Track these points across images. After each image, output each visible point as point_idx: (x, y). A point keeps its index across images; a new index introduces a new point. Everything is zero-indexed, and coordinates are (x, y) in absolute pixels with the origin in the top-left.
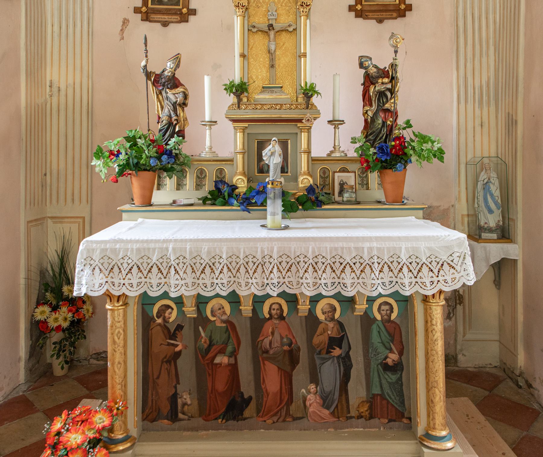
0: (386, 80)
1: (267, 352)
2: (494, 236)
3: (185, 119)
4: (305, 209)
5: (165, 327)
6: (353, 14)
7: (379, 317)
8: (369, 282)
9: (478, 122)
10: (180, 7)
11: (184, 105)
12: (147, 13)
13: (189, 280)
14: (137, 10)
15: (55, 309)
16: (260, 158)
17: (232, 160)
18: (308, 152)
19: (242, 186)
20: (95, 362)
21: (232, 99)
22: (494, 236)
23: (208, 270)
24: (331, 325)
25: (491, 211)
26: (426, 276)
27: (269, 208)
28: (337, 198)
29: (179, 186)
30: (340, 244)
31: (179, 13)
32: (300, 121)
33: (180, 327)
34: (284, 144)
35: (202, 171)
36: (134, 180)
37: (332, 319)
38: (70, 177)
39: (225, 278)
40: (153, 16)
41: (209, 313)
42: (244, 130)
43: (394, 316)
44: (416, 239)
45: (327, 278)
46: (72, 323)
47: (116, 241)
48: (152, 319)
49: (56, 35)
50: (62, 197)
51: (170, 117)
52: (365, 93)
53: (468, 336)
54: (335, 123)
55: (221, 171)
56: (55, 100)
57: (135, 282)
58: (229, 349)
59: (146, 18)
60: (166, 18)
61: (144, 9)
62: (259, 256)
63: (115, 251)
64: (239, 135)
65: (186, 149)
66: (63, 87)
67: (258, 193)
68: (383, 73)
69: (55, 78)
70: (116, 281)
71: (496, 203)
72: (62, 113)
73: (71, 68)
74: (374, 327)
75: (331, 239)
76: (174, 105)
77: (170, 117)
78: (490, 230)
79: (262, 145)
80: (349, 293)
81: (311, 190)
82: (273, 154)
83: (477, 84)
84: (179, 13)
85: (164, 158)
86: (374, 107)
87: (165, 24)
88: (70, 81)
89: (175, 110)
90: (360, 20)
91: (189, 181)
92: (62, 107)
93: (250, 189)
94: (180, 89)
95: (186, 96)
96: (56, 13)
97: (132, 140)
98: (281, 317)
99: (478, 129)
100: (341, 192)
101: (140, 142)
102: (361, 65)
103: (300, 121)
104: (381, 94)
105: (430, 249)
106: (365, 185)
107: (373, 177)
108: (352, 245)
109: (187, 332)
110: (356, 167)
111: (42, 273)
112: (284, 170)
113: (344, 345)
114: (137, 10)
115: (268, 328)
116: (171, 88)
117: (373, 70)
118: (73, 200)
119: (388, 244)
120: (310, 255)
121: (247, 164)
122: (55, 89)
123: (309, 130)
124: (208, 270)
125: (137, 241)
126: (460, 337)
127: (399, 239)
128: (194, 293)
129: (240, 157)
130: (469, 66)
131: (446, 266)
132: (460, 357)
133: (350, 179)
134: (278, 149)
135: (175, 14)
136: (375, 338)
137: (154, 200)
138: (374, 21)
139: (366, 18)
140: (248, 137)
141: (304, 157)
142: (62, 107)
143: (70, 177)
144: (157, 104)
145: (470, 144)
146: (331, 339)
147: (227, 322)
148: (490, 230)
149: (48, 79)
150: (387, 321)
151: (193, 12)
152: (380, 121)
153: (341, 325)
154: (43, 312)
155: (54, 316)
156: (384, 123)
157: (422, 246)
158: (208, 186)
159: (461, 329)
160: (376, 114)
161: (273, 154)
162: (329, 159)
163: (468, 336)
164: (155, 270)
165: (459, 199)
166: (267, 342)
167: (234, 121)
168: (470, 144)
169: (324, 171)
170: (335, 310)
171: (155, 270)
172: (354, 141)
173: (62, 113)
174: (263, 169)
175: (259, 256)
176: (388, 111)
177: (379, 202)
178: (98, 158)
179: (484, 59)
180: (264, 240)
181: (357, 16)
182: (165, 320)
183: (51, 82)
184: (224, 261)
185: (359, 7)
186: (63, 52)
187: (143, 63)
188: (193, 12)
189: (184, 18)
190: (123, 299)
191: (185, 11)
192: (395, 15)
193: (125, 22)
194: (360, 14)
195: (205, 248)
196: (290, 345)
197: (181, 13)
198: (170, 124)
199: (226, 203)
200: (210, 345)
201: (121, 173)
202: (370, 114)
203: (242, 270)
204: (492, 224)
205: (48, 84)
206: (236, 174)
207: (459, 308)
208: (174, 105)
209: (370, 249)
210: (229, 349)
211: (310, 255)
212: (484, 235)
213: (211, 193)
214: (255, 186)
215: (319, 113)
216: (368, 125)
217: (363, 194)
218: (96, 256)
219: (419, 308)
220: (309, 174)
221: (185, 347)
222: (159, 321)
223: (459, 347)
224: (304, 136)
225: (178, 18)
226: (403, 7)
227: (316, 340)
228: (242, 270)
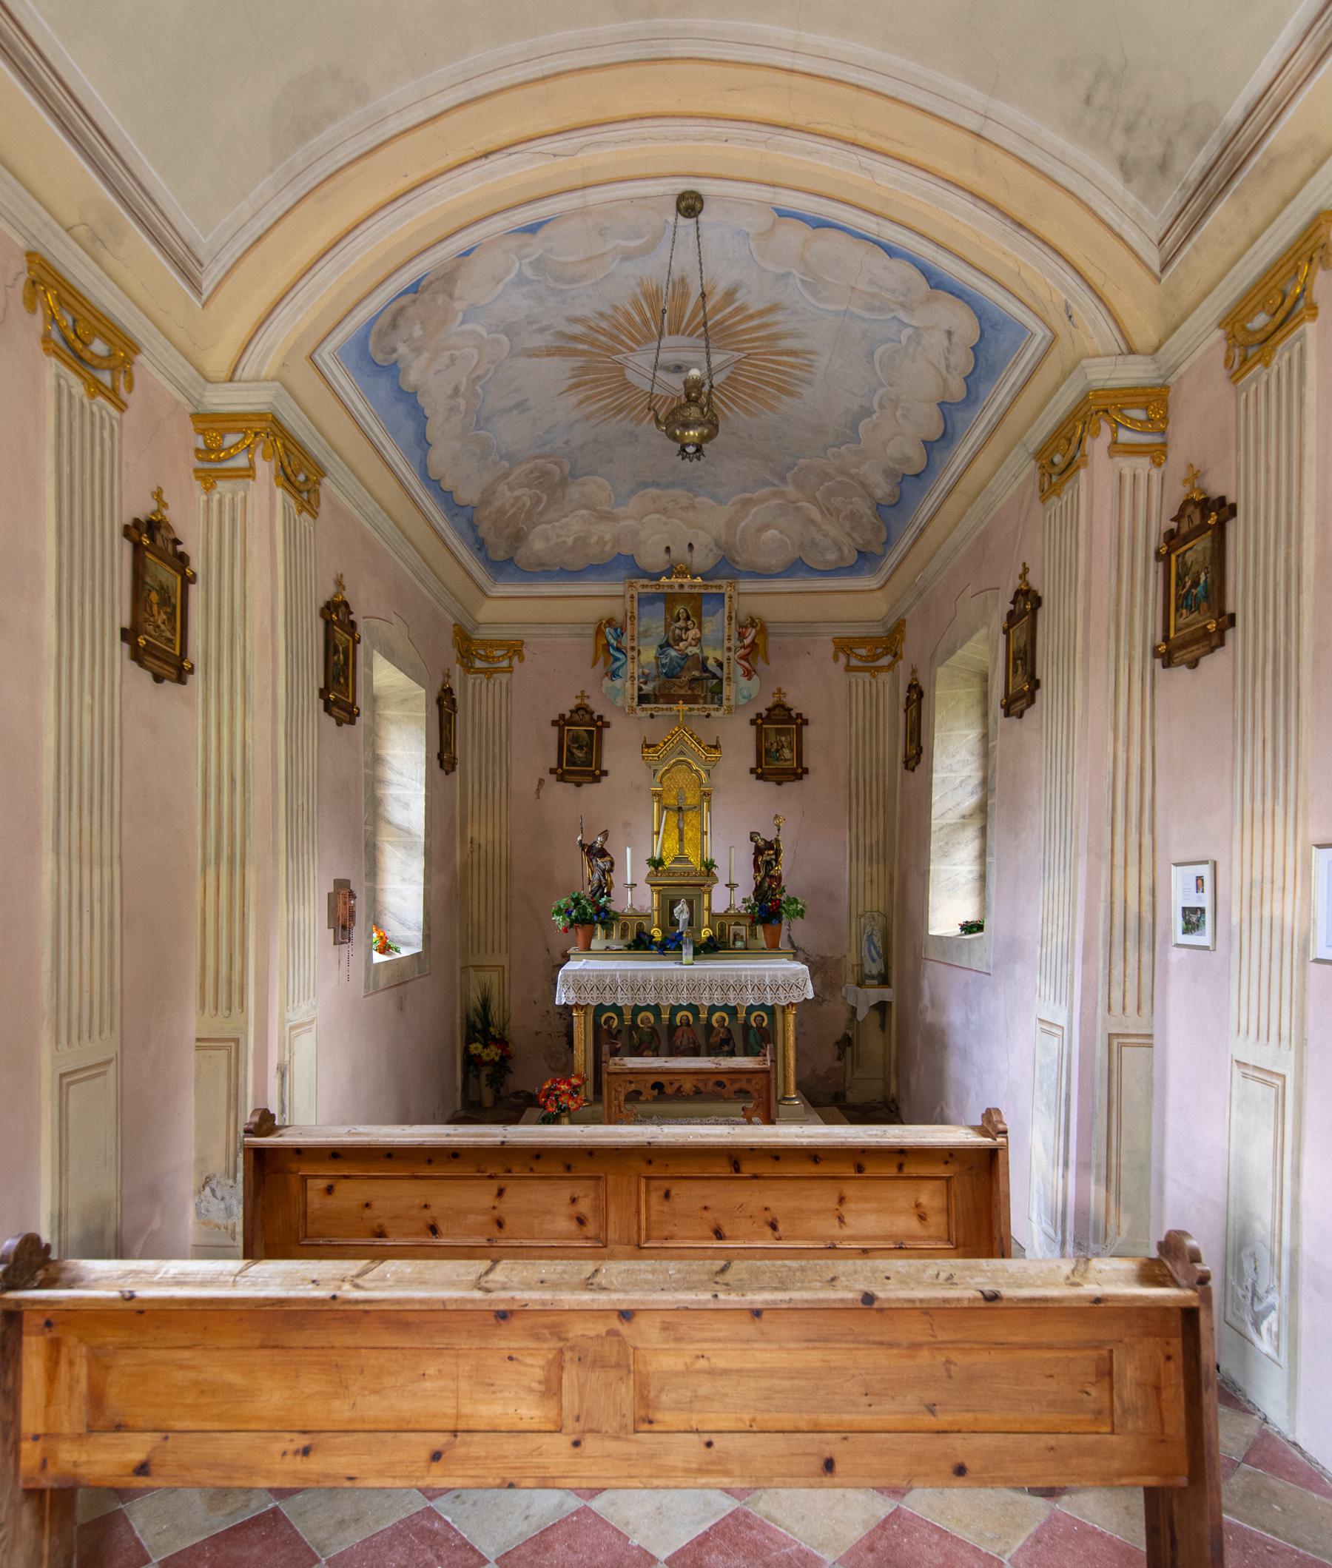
0: (771, 852)
1: (678, 1048)
2: (876, 982)
3: (612, 882)
4: (706, 953)
5: (609, 1031)
6: (754, 776)
7: (754, 1025)
8: (745, 997)
9: (868, 878)
10: (593, 768)
11: (611, 870)
12: (562, 774)
13: (630, 996)
14: (552, 771)
15: (485, 1046)
16: (672, 913)
17: (649, 916)
18: (709, 909)
19: (657, 934)
20: (515, 1100)
21: (650, 869)
22: (876, 982)
23: (642, 989)
24: (722, 1030)
25: (873, 960)
26: (781, 993)
27: (684, 951)
28: (732, 946)
29: (608, 936)
30: (727, 973)
31: (592, 774)
32: (703, 885)
33: (619, 1031)
34: (690, 903)
35: (625, 925)
36: (579, 931)
37: (723, 1026)
38: (490, 928)
39: (653, 994)
40: (568, 777)
41: (639, 1022)
42: (659, 892)
43: (764, 1024)
44: (776, 969)
45: (717, 995)
46: (502, 1057)
47: (583, 970)
48: (601, 1026)
49: (476, 795)
50: (489, 948)
51: (600, 880)
52: (755, 861)
53: (856, 1075)
54: (731, 886)
55: (640, 924)
56: (476, 855)
57: (595, 996)
58: (653, 1046)
59: (561, 778)
60: (580, 779)
61: (560, 771)
62: (675, 980)
63: (581, 976)
64: (655, 896)
65: (615, 907)
66: (483, 843)
67: (672, 941)
68: (769, 845)
69: (476, 835)
70: (583, 996)
71: (878, 953)
72: (483, 868)
73: (490, 826)
74: (752, 1032)
75: (721, 969)
76: (604, 872)
77: (600, 880)
78: (873, 977)
79: (673, 904)
80: (732, 1004)
81: (710, 939)
82: (682, 912)
83: (868, 843)
84: (592, 774)
85: (603, 914)
86: (762, 873)
87: (578, 785)
88: (490, 838)
89: (604, 876)
90: (761, 783)
91: (616, 933)
92: (482, 863)
93: (664, 938)
94: (608, 858)
95: (612, 864)
96: (476, 773)
97: (577, 901)
98: (688, 1025)
99: (868, 884)
100: (735, 940)
101: (583, 902)
102: (752, 839)
103: (703, 885)
104: (768, 863)
105: (784, 975)
106: (754, 935)
107: (759, 928)
108: (734, 973)
109: (624, 1035)
110: (748, 921)
111: (467, 1018)
112: (690, 924)
113: (731, 1044)
114: (552, 771)
115: (679, 1032)
116: (600, 858)
117: (761, 843)
118: (493, 951)
119: (758, 973)
120: (707, 979)
121: (661, 918)
122: (476, 846)
123: (710, 893)
124: (642, 989)
125: (596, 970)
126: (848, 1076)
127: (765, 969)
128: (633, 1004)
129: (656, 913)
130: (861, 826)
131: (794, 987)
132: (848, 1094)
133: (743, 930)
134: (686, 907)
135: (588, 775)
136: (752, 1039)
137: (592, 947)
138: (774, 783)
139: (766, 780)
140: (662, 898)
141: (706, 914)
142: (482, 863)
143: (490, 928)
144: (588, 871)
145: (861, 898)
146: (722, 1039)
147: (652, 1028)
148: (873, 977)
149: (469, 836)
150: (760, 1027)
151: (605, 773)
152: (766, 885)
153: (728, 1030)
154: (476, 1048)
155: (486, 1051)
156: (770, 886)
157: (779, 974)
158: (631, 936)
159: (849, 1068)
160: (763, 879)
161: (682, 912)
162: (726, 915)
163: (856, 1075)
164: (608, 988)
165: (850, 950)
166: (678, 1043)
167: (652, 885)
168: (861, 898)
169: (722, 925)
170: (724, 1020)
171: (608, 988)
172: (744, 901)
173: (483, 868)
174: (674, 923)
175: (675, 980)
176: (772, 877)
177: (763, 949)
178: (558, 915)
179: (874, 821)
180: (678, 969)
181: (757, 778)
182: (610, 1027)
183: (472, 838)
184: (652, 983)
185: (759, 771)
186: (483, 810)
187: (579, 838)
188: (605, 773)
189: (597, 780)
190: (582, 1008)
191: (597, 772)
192: (793, 778)
193: (541, 782)
194: (760, 777)
195: (640, 975)
196: (694, 1043)
197: (594, 775)
198: (600, 886)
199: (647, 948)
200: (640, 1044)
201: (571, 926)
202: (759, 878)
203: (664, 989)
204: (875, 972)
205: (469, 840)
206: (653, 927)
207: (849, 1050)
208: (604, 872)
209: (746, 976)
210: (653, 1046)
211: (707, 979)
212: (868, 982)
213: (634, 941)
214: (668, 935)
215: (717, 879)
216: (758, 889)
217: (752, 943)
218: (571, 979)
219: (779, 1015)
220: (709, 926)
221: (623, 1045)
222: (605, 1027)
223: (847, 1085)
224: (706, 896)
225: (591, 778)
226: (800, 771)
227: (712, 1041)
228: (664, 989)
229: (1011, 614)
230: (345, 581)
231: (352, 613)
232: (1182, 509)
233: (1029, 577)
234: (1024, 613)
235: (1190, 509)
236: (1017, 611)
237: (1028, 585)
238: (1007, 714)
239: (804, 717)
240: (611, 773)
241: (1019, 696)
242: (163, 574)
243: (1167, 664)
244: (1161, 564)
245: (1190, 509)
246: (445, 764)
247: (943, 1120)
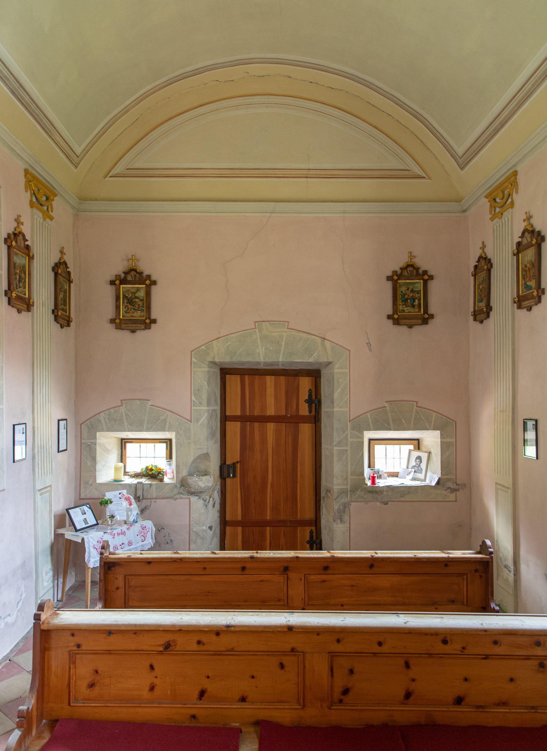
60: (134, 326)
84: (143, 322)
87: (133, 331)
151: (154, 321)
188: (154, 321)
191: (148, 321)
229: (519, 244)
230: (65, 251)
231: (69, 268)
232: (523, 233)
233: (532, 221)
234: (529, 245)
235: (526, 234)
236: (524, 243)
237: (532, 226)
238: (475, 320)
239: (429, 274)
240: (159, 283)
241: (481, 311)
242: (20, 260)
243: (519, 307)
244: (515, 257)
245: (526, 234)
246: (13, 301)
247: (321, 549)
